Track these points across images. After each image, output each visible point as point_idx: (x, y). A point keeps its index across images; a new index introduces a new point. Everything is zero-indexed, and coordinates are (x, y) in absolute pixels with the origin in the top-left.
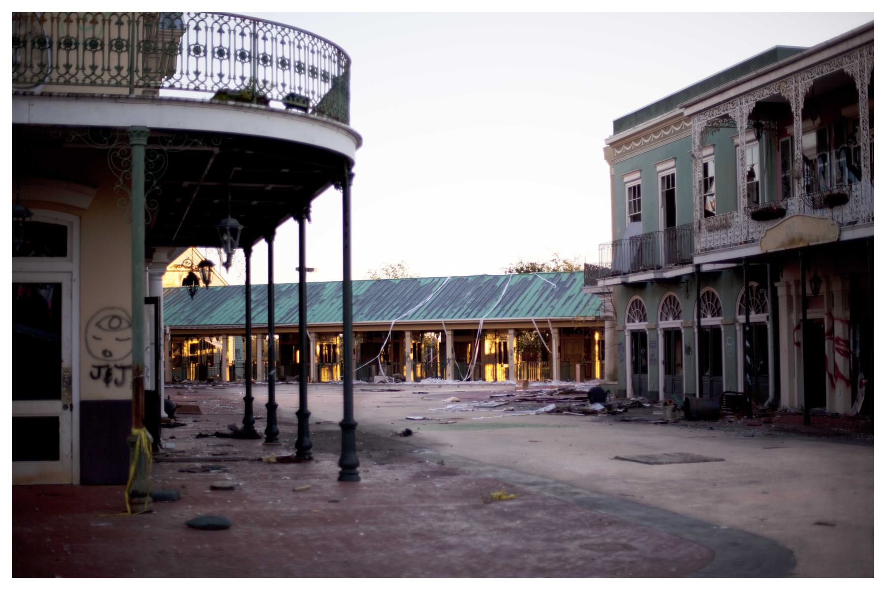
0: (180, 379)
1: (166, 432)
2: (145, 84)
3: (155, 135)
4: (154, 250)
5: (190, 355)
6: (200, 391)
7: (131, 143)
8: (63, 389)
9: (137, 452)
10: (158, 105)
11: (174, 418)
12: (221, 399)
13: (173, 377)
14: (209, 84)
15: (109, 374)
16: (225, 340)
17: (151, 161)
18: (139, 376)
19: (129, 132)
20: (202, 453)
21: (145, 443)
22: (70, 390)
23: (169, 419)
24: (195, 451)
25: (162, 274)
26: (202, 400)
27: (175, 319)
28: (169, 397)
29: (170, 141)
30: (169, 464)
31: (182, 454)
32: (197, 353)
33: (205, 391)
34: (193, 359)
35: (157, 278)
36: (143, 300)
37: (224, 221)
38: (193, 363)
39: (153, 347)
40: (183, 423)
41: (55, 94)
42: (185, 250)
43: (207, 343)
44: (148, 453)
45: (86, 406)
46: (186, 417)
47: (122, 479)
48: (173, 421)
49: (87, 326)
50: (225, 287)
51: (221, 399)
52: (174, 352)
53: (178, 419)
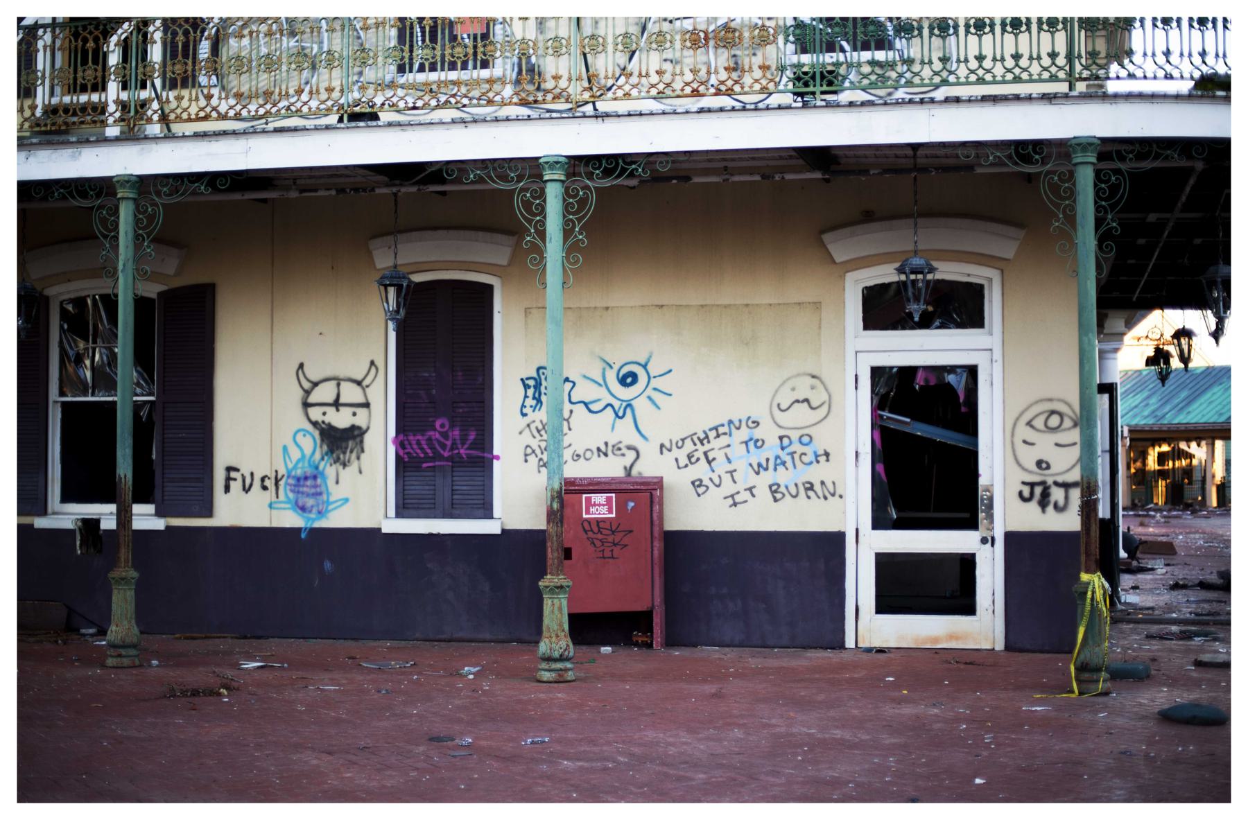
0: (1144, 502)
1: (1126, 580)
2: (1092, 75)
3: (1109, 148)
4: (1106, 316)
5: (1157, 467)
6: (1173, 521)
7: (1075, 161)
8: (981, 515)
9: (1088, 608)
10: (1111, 104)
11: (1137, 560)
12: (1205, 533)
13: (1133, 501)
14: (1187, 69)
15: (1045, 495)
16: (1210, 447)
17: (1103, 186)
18: (1090, 497)
19: (1071, 146)
20: (1180, 611)
21: (1099, 594)
22: (990, 517)
23: (1129, 560)
24: (1169, 608)
25: (1116, 350)
26: (1177, 535)
27: (1135, 416)
28: (1129, 528)
29: (1131, 156)
30: (1131, 626)
31: (1150, 612)
32: (1168, 465)
33: (1181, 521)
34: (1162, 474)
35: (1111, 355)
36: (1095, 389)
37: (1212, 269)
38: (1162, 479)
39: (1107, 456)
40: (1150, 567)
41: (964, 98)
42: (1144, 317)
43: (1183, 450)
44: (1104, 609)
45: (1012, 539)
46: (1154, 559)
47: (1065, 646)
48: (1135, 563)
49: (1015, 425)
50: (1208, 368)
51: (1205, 533)
52: (1134, 463)
53: (1143, 561)
